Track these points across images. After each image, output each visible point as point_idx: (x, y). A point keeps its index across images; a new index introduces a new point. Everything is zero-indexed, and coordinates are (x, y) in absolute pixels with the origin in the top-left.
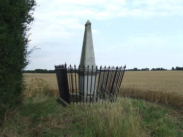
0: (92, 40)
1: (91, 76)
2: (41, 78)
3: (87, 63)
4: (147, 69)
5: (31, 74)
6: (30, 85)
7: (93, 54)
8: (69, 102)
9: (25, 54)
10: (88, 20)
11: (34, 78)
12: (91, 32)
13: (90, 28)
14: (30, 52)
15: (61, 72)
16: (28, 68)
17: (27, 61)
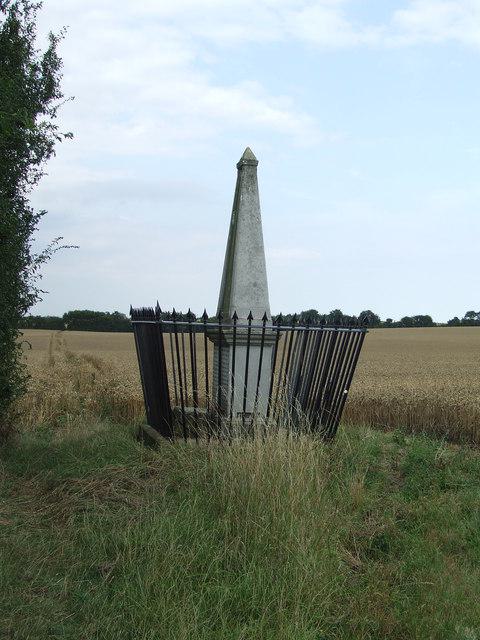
0: (260, 223)
1: (245, 349)
2: (89, 353)
3: (241, 306)
4: (424, 321)
5: (48, 333)
6: (41, 381)
7: (262, 272)
8: (167, 434)
9: (22, 265)
10: (248, 149)
11: (59, 355)
12: (255, 192)
13: (253, 178)
14: (41, 259)
15: (150, 329)
16: (35, 311)
17: (32, 292)
